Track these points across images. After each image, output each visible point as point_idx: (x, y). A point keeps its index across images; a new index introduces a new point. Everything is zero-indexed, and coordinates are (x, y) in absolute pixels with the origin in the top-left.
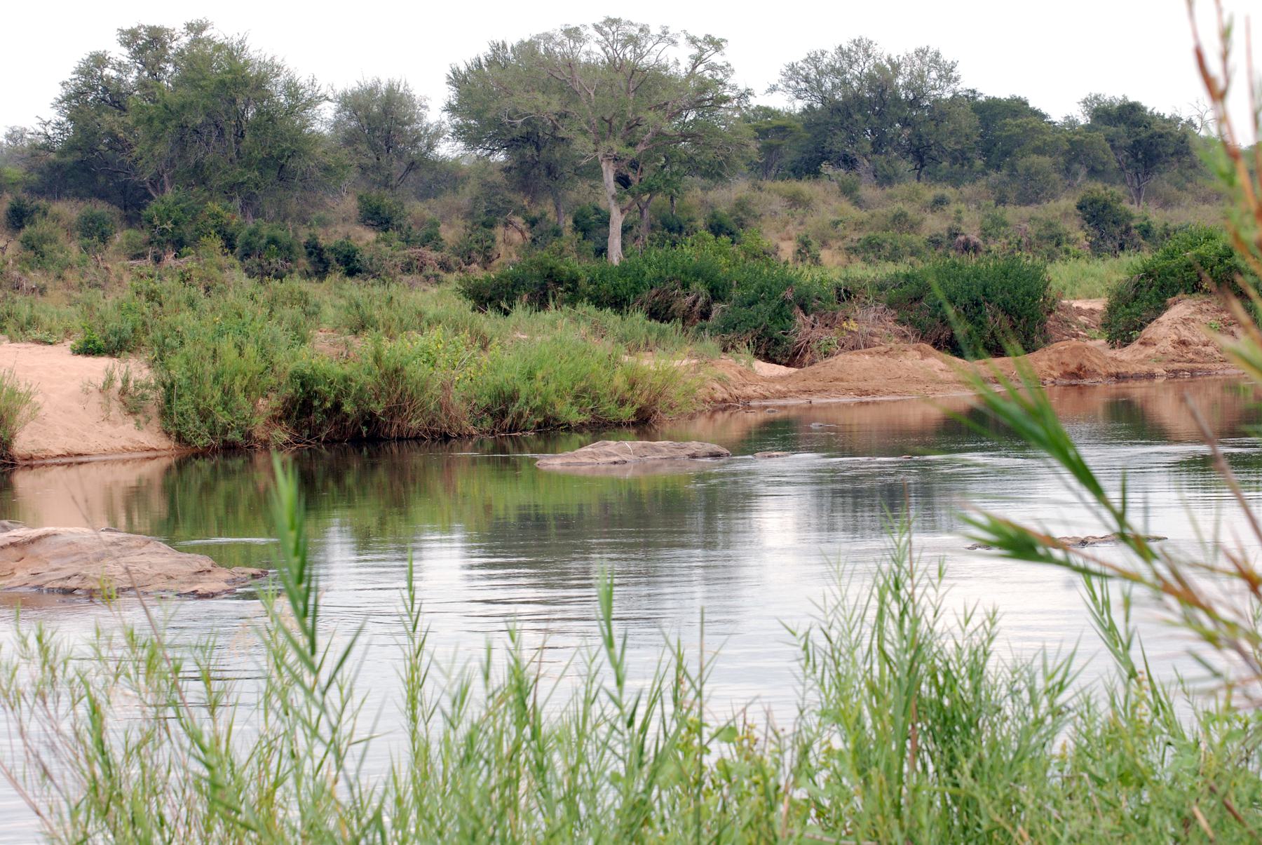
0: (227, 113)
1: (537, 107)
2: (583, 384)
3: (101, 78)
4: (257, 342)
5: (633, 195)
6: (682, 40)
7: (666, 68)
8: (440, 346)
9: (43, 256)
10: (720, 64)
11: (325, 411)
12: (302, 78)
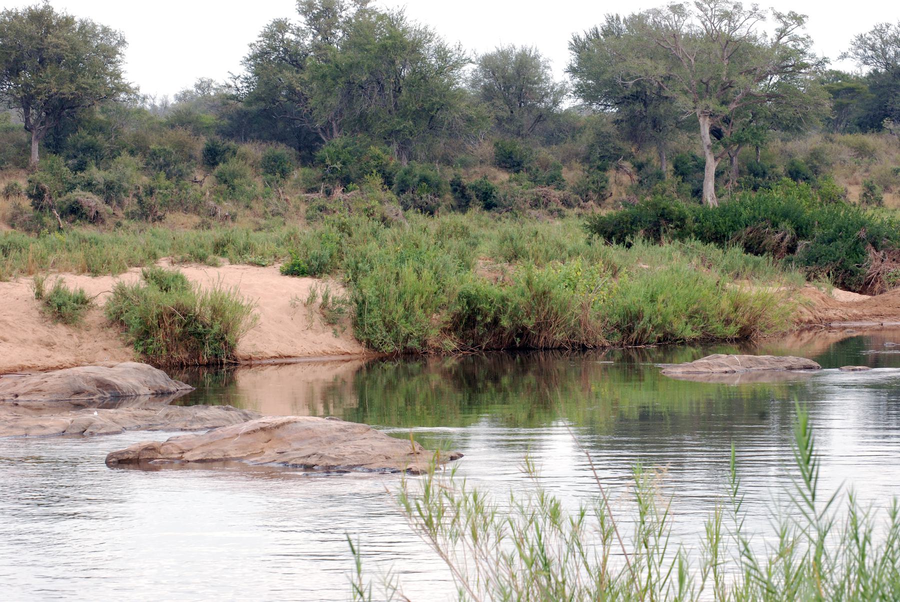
0: (387, 72)
1: (646, 71)
2: (695, 306)
3: (282, 41)
4: (431, 267)
5: (725, 146)
6: (770, 16)
7: (755, 39)
8: (579, 273)
9: (234, 189)
10: (801, 36)
11: (486, 325)
12: (450, 44)
